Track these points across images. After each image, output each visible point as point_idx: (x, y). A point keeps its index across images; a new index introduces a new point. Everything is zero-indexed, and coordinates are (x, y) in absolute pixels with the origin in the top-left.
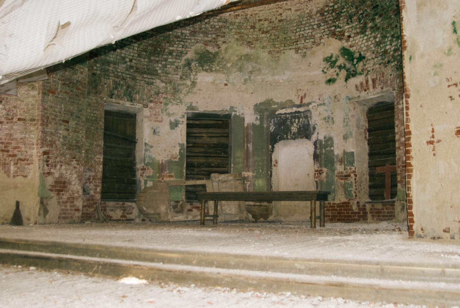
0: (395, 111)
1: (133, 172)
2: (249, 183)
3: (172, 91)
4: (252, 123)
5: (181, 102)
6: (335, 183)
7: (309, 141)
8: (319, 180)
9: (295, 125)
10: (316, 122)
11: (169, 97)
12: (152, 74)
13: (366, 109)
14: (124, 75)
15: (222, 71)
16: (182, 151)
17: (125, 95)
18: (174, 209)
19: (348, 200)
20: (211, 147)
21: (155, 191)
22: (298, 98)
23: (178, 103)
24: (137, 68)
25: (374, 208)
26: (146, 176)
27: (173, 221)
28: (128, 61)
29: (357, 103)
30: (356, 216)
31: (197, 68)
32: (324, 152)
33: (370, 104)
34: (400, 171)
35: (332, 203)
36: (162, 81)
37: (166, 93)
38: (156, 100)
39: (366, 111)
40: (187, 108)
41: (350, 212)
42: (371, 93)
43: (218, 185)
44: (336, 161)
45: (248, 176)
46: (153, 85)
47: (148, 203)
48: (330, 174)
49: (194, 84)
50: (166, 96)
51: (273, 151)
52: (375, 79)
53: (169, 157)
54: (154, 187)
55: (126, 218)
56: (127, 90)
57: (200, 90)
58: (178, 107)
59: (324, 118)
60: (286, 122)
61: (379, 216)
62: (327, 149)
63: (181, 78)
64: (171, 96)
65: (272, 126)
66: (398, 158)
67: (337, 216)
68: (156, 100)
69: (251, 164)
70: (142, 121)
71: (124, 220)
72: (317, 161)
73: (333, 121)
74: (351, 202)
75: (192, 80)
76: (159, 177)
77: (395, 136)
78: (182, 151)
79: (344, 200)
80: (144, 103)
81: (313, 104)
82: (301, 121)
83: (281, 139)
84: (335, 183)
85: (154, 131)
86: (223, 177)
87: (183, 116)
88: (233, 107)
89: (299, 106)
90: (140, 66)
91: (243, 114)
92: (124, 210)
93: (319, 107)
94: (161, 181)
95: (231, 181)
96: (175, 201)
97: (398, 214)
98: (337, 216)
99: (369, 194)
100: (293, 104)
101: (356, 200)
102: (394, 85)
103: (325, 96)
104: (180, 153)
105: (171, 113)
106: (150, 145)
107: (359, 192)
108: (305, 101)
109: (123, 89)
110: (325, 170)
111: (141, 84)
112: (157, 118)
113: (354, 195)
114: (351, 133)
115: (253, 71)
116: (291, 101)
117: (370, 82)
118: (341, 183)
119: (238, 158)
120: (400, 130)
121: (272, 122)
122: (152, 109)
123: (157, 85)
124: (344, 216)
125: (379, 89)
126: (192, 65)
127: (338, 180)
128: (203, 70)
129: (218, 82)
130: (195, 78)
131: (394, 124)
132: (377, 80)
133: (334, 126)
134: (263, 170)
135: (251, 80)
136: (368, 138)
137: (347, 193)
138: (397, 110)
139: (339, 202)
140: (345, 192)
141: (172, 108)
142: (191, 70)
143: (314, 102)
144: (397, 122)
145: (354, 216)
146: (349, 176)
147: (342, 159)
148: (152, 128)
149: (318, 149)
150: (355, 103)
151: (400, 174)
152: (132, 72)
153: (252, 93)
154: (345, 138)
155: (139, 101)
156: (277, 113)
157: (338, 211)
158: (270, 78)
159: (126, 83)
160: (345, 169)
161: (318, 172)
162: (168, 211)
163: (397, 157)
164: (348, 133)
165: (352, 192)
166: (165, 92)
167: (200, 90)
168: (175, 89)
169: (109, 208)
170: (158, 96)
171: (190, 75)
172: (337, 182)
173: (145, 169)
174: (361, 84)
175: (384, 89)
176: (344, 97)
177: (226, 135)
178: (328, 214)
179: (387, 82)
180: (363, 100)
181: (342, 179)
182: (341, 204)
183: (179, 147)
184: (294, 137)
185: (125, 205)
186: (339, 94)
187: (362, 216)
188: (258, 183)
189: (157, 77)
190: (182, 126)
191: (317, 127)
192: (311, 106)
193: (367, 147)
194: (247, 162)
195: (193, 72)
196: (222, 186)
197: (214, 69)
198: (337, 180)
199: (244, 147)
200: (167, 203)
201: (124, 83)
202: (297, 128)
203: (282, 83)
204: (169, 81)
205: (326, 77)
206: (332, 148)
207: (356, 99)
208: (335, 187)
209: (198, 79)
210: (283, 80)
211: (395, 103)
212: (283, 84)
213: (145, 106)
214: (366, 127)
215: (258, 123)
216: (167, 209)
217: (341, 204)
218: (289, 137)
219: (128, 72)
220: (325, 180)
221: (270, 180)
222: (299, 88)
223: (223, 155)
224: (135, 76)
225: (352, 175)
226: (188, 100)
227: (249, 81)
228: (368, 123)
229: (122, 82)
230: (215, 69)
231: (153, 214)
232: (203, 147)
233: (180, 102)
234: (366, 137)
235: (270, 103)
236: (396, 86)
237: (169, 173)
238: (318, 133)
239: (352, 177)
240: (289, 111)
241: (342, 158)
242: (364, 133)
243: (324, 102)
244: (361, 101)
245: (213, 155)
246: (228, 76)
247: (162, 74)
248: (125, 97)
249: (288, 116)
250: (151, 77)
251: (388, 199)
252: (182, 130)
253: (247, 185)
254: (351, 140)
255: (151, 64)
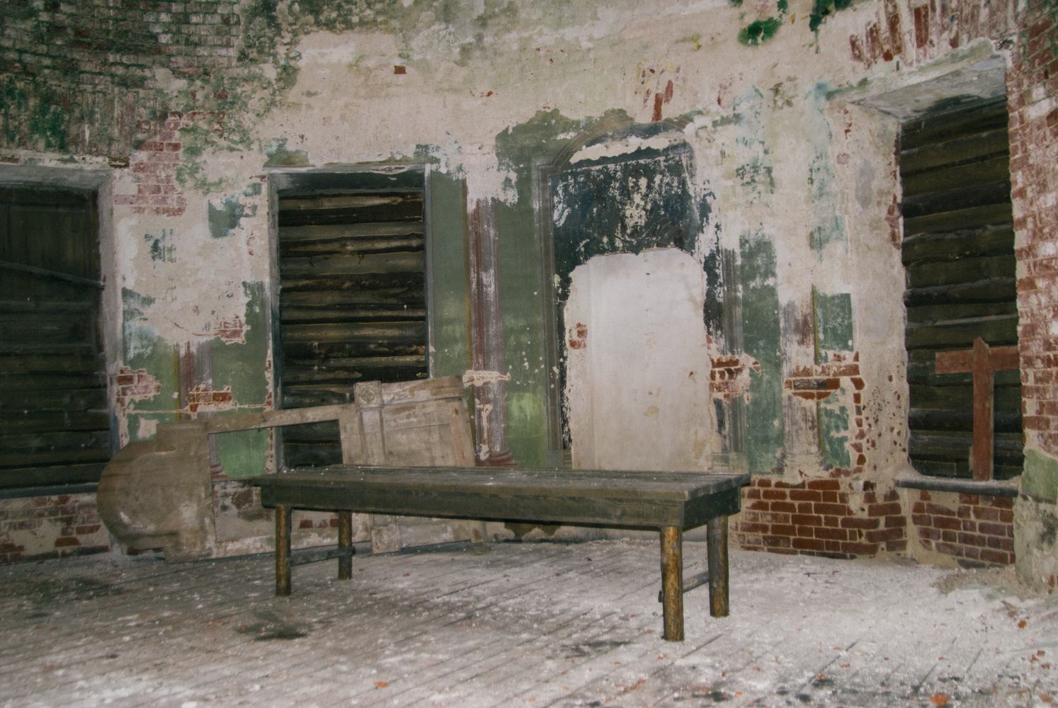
0: (1011, 130)
1: (96, 391)
2: (489, 407)
3: (213, 103)
4: (493, 199)
5: (246, 140)
6: (785, 410)
7: (688, 255)
8: (726, 396)
9: (637, 198)
10: (712, 187)
11: (203, 125)
12: (136, 50)
13: (894, 128)
14: (28, 58)
15: (386, 22)
16: (257, 310)
17: (35, 128)
18: (238, 506)
19: (832, 475)
20: (363, 288)
21: (164, 453)
22: (645, 101)
23: (235, 142)
24: (78, 33)
25: (930, 506)
26: (132, 401)
27: (221, 555)
28: (41, 7)
29: (856, 108)
30: (861, 535)
31: (297, 19)
32: (740, 295)
33: (909, 109)
34: (1037, 380)
35: (773, 483)
36: (177, 73)
37: (192, 110)
38: (158, 139)
39: (894, 138)
40: (266, 158)
41: (840, 518)
42: (911, 64)
43: (382, 420)
44: (785, 330)
45: (486, 384)
46: (142, 86)
47: (137, 499)
48: (766, 377)
49: (288, 74)
50: (191, 124)
51: (565, 296)
52: (925, 7)
53: (212, 331)
54: (160, 441)
55: (75, 547)
56: (43, 111)
57: (309, 94)
58: (234, 158)
59: (737, 170)
60: (606, 189)
61: (947, 537)
62: (752, 284)
63: (243, 57)
64: (210, 123)
65: (560, 206)
66: (1025, 326)
67: (791, 530)
68: (158, 139)
69: (494, 343)
70: (112, 214)
71: (70, 555)
72: (719, 327)
73: (772, 179)
74: (843, 481)
75: (282, 62)
76: (180, 403)
77: (1011, 235)
78: (257, 310)
79: (817, 472)
80: (114, 153)
81: (699, 121)
82: (656, 186)
83: (590, 252)
84: (785, 410)
85: (155, 247)
86: (395, 392)
87: (256, 190)
88: (426, 147)
89: (651, 131)
90: (89, 26)
91: (460, 169)
92: (69, 521)
93: (719, 128)
94: (188, 417)
95: (424, 404)
96: (239, 481)
97: (1029, 553)
98: (791, 530)
99: (911, 450)
100: (628, 123)
101: (860, 475)
102: (1006, 23)
103: (741, 90)
104: (250, 315)
105: (212, 178)
106: (143, 295)
107: (874, 445)
108: (669, 111)
109: (27, 109)
110: (746, 360)
111: (99, 88)
112: (164, 199)
113: (854, 456)
114: (837, 225)
115: (492, 16)
116: (621, 114)
117: (907, 24)
118: (804, 409)
119: (450, 322)
120: (1034, 208)
121: (560, 192)
122: (142, 170)
123: (160, 85)
124: (819, 533)
125: (940, 47)
126: (278, 8)
127: (796, 399)
128: (318, 23)
129: (371, 63)
130: (292, 55)
131: (1008, 185)
132: (934, 9)
133: (773, 198)
134: (534, 363)
135: (483, 49)
136: (901, 240)
137: (828, 447)
138: (1017, 126)
139: (799, 480)
140: (820, 445)
141: (215, 163)
142: (278, 27)
143: (700, 113)
144: (1019, 179)
145: (853, 536)
146: (834, 384)
147: (805, 322)
148: (146, 236)
149: (721, 285)
150: (849, 107)
151: (1037, 390)
152: (60, 47)
153: (490, 94)
154: (817, 241)
155: (92, 144)
156: (574, 159)
157: (797, 513)
158: (546, 38)
159: (37, 85)
160: (817, 358)
161: (722, 369)
162: (207, 521)
163: (1023, 321)
164: (827, 225)
165: (847, 445)
166: (188, 108)
167: (309, 94)
168: (221, 96)
169: (9, 521)
170: (162, 125)
171: (273, 46)
172: (790, 406)
173: (129, 380)
174: (873, 33)
175: (965, 46)
176: (809, 87)
177: (414, 243)
178: (760, 522)
179: (973, 16)
180: (880, 97)
181: (807, 396)
182: (807, 489)
183: (246, 295)
184: (635, 243)
185: (69, 504)
186: (790, 79)
187: (884, 536)
188: (520, 408)
189: (157, 57)
190: (253, 221)
191: (714, 204)
192: (689, 129)
193: (899, 273)
194: (481, 334)
195: (283, 33)
196: (393, 424)
197: (355, 19)
198: (790, 398)
199: (470, 283)
200: (203, 495)
201: (31, 87)
202: (644, 209)
203: (589, 50)
204: (201, 70)
205: (742, 17)
206: (770, 282)
207: (853, 92)
208: (783, 424)
209: (304, 55)
210: (591, 39)
211: (1013, 99)
212: (592, 55)
213: (118, 163)
214: (895, 198)
215: (511, 197)
216: (201, 516)
217: (807, 489)
218: (619, 243)
219: (43, 48)
220: (747, 398)
221: (558, 398)
222: (646, 66)
223: (405, 314)
224: (72, 59)
225: (846, 381)
226: (271, 130)
227: (477, 53)
228: (903, 183)
229: (20, 85)
230: (361, 20)
231: (154, 536)
232: (338, 289)
233: (242, 141)
234: (894, 237)
235: (549, 123)
236: (1013, 28)
237: (214, 387)
238: (718, 227)
239: (843, 391)
240: (616, 149)
241: (805, 317)
242: (887, 219)
243: (737, 112)
244: (873, 99)
245: (362, 314)
246: (406, 40)
247: (174, 49)
248: (37, 136)
249: (611, 167)
250: (133, 62)
251: (982, 478)
252: (252, 237)
253: (484, 415)
254: (837, 248)
255: (130, 14)
